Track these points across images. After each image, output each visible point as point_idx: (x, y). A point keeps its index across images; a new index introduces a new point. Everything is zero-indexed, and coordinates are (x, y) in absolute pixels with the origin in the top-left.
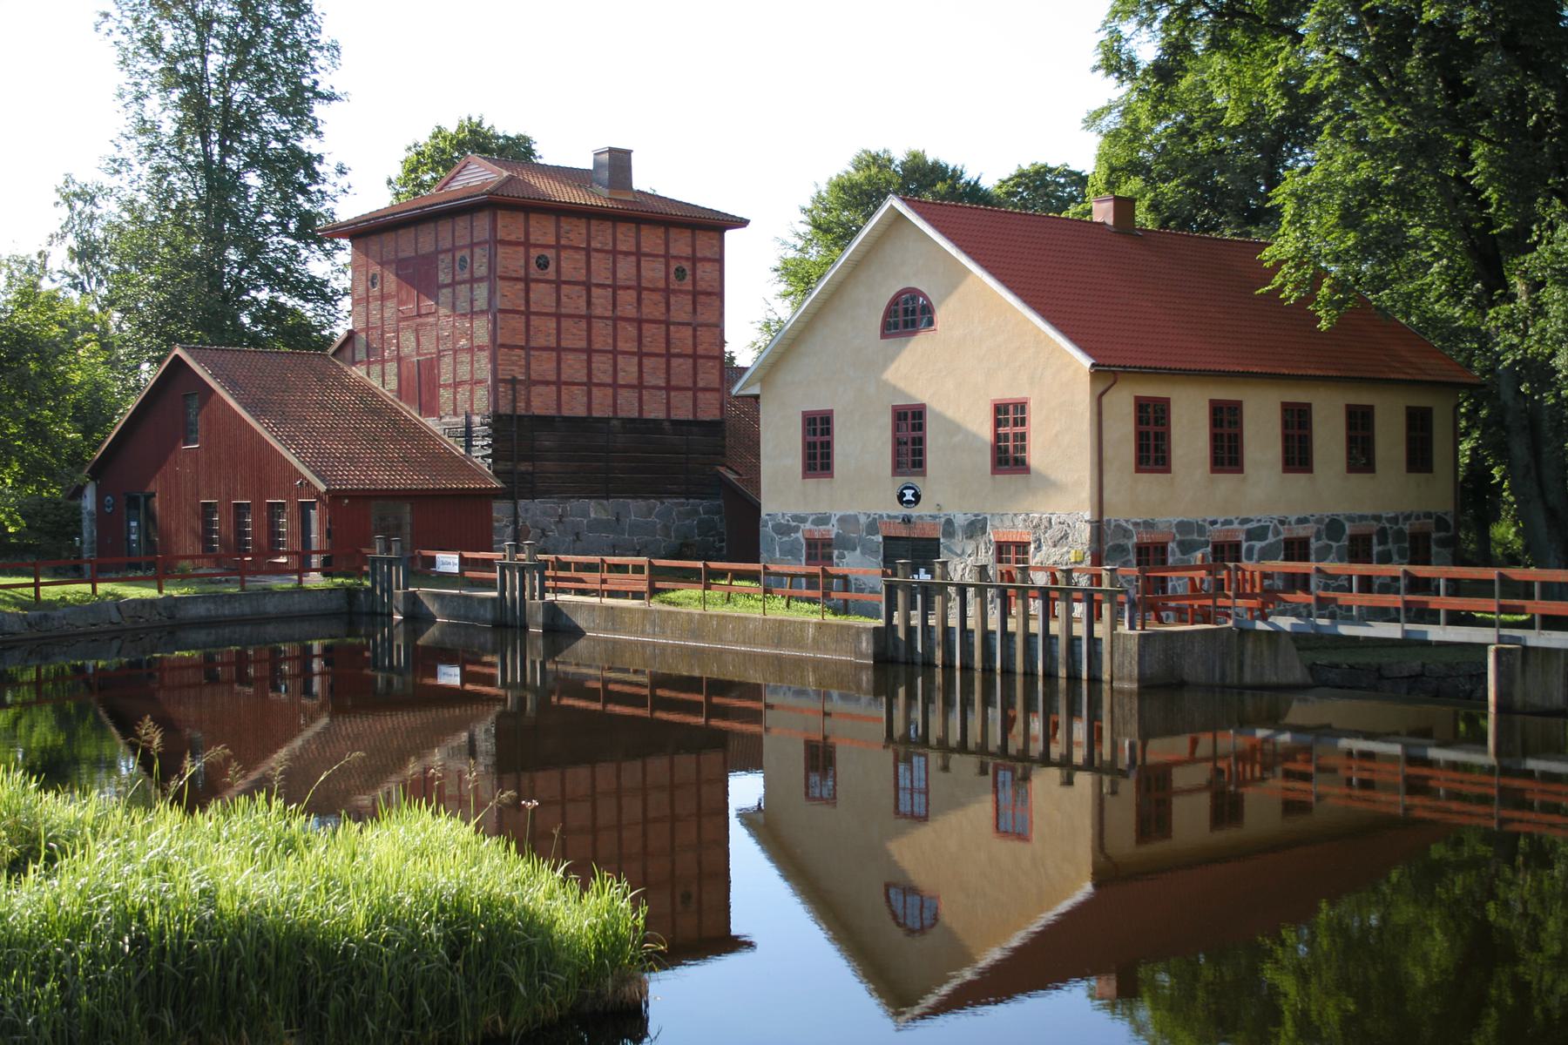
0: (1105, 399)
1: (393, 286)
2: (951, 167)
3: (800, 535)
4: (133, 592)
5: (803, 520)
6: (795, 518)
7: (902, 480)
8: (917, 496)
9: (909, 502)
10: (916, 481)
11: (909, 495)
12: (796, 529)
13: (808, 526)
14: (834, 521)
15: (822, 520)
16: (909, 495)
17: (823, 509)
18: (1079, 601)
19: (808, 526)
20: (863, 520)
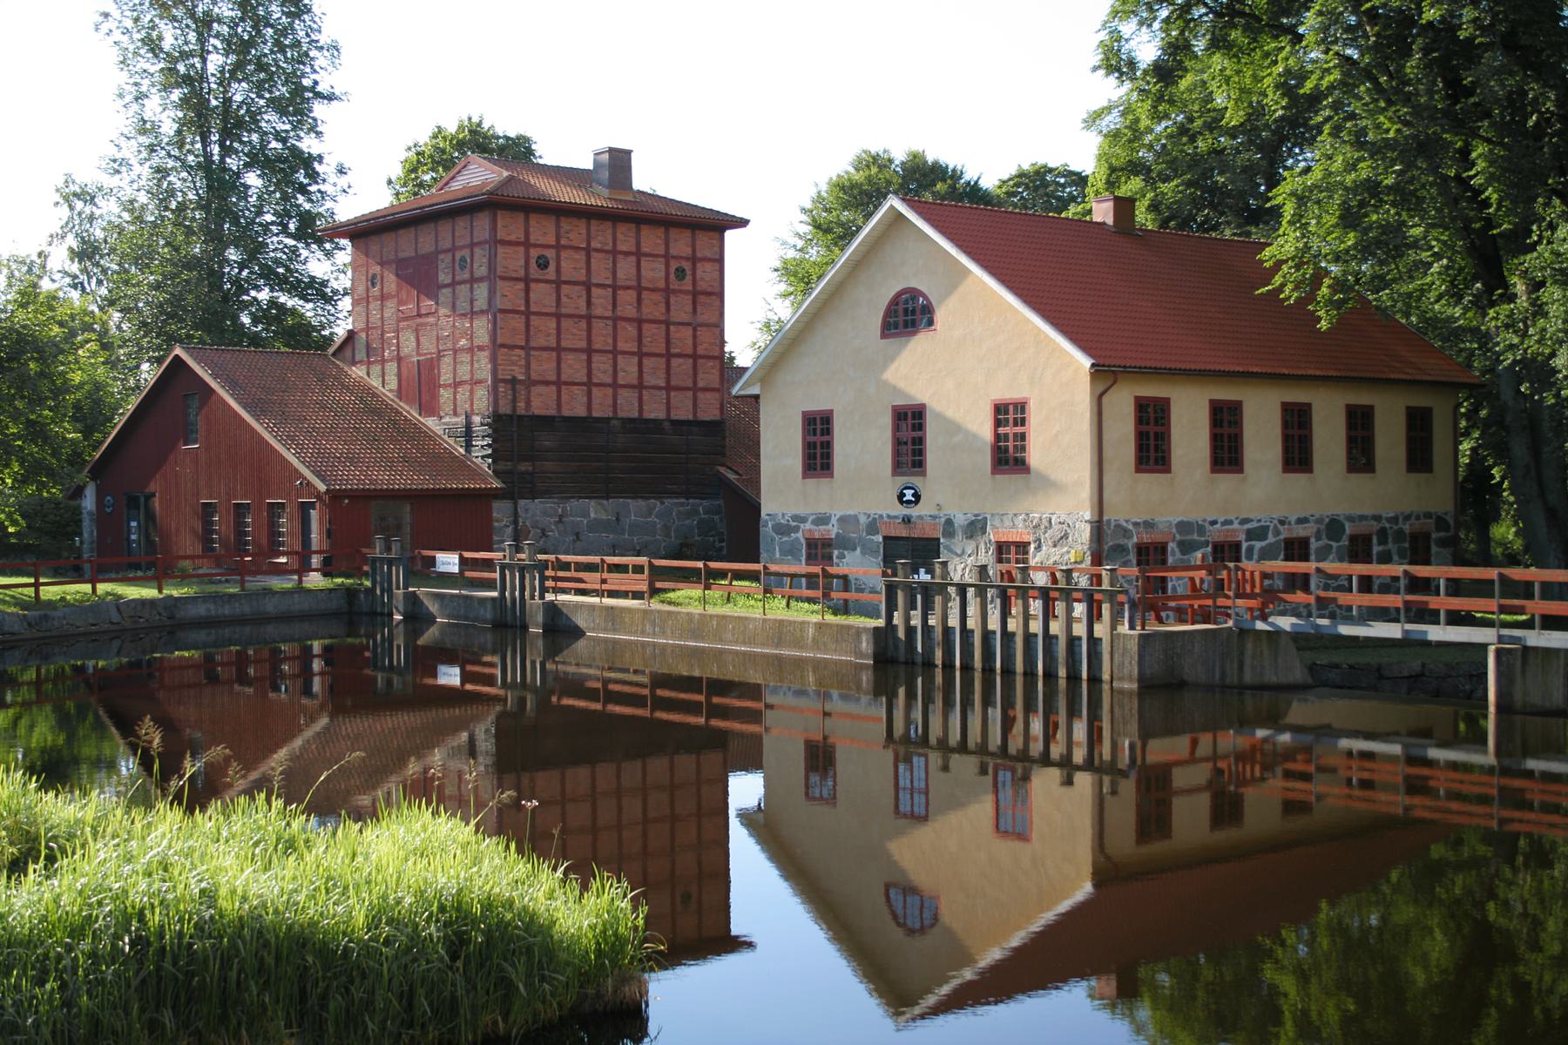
2: (951, 167)
3: (800, 535)
4: (133, 592)
5: (803, 520)
6: (795, 518)
7: (902, 480)
8: (917, 496)
9: (909, 502)
10: (916, 481)
11: (909, 495)
12: (796, 529)
13: (808, 526)
14: (834, 521)
15: (822, 520)
16: (909, 495)
17: (823, 509)
19: (808, 526)
20: (863, 520)
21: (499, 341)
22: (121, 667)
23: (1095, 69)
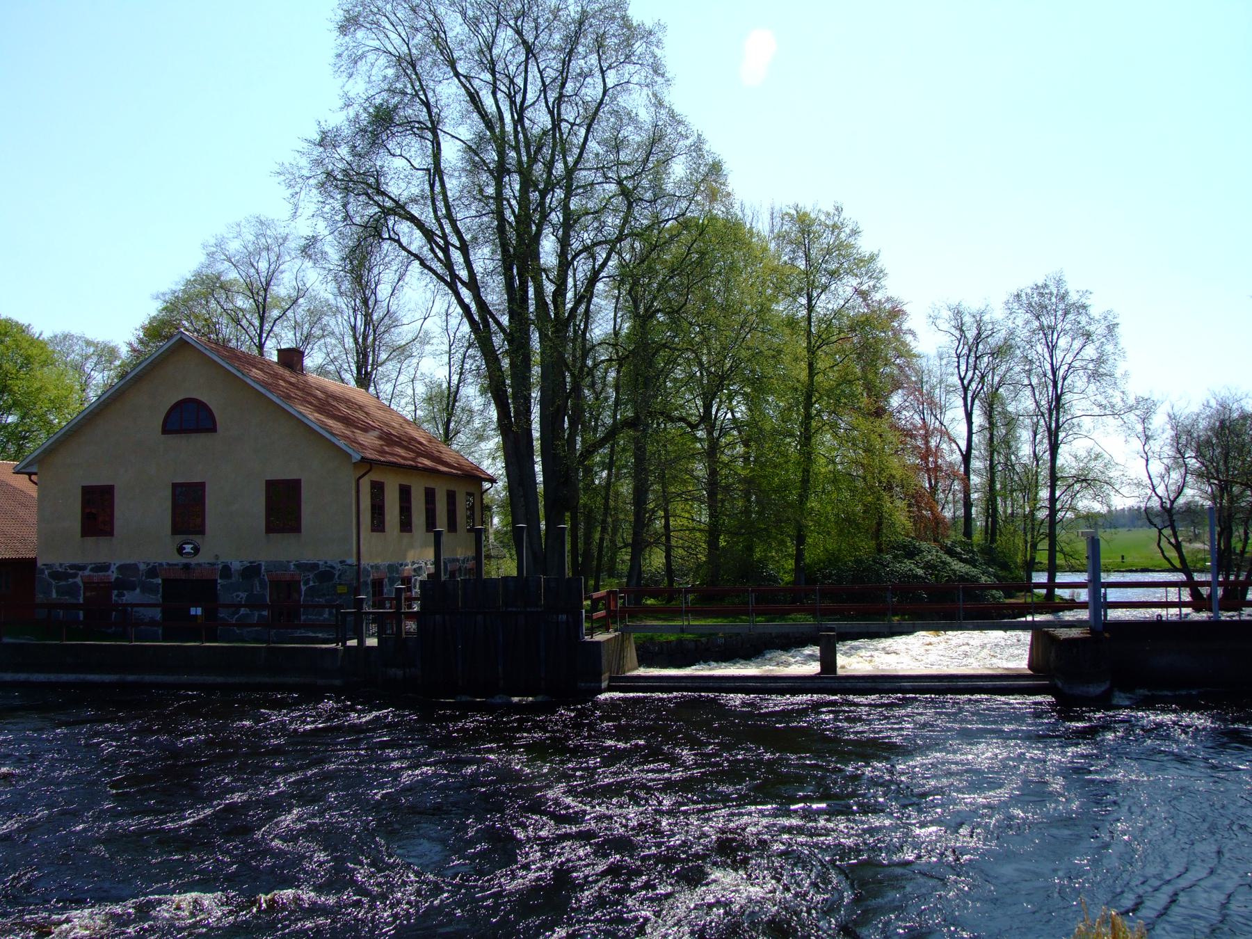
0: (361, 481)
1: (509, 45)
2: (729, 189)
3: (78, 580)
4: (538, 468)
5: (83, 568)
6: (73, 567)
7: (179, 538)
8: (197, 550)
9: (189, 553)
10: (197, 539)
11: (188, 548)
12: (75, 576)
13: (87, 573)
14: (113, 568)
15: (104, 567)
16: (188, 548)
17: (102, 559)
18: (1106, 615)
19: (87, 573)
20: (142, 567)
21: (1104, 535)
22: (251, 708)
23: (839, 210)
